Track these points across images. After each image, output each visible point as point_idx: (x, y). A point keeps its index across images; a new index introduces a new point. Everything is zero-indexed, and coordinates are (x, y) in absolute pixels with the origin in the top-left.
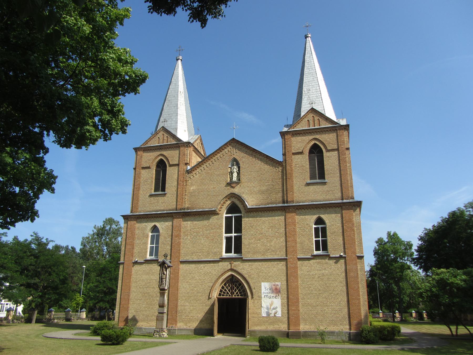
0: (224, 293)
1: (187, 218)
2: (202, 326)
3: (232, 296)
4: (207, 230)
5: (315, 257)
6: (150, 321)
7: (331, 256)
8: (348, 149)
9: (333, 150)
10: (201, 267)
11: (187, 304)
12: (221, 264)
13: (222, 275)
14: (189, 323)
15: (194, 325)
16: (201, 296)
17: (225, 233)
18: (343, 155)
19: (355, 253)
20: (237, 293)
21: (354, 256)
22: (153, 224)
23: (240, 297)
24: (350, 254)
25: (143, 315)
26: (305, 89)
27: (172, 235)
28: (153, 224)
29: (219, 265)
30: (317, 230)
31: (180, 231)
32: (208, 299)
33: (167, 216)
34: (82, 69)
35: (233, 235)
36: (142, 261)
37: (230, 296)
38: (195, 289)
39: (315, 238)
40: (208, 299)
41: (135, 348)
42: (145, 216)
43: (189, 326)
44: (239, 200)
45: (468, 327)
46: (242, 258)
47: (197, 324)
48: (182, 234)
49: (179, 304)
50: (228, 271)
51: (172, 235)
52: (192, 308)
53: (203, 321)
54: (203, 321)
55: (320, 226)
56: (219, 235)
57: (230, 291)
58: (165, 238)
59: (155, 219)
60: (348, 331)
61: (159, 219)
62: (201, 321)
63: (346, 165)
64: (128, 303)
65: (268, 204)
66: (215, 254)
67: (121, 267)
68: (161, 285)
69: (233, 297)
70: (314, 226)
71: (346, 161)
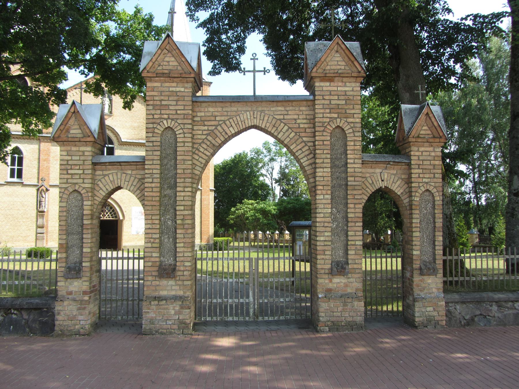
5: (8, 183)
7: (24, 183)
19: (209, 187)
20: (109, 215)
21: (208, 189)
23: (111, 218)
24: (205, 188)
25: (7, 236)
27: (39, 159)
31: (49, 156)
34: (426, 23)
36: (4, 183)
42: (16, 136)
44: (113, 132)
46: (22, 183)
48: (51, 159)
51: (39, 159)
59: (17, 140)
60: (199, 243)
61: (22, 140)
65: (139, 139)
67: (199, 193)
68: (40, 208)
69: (105, 218)
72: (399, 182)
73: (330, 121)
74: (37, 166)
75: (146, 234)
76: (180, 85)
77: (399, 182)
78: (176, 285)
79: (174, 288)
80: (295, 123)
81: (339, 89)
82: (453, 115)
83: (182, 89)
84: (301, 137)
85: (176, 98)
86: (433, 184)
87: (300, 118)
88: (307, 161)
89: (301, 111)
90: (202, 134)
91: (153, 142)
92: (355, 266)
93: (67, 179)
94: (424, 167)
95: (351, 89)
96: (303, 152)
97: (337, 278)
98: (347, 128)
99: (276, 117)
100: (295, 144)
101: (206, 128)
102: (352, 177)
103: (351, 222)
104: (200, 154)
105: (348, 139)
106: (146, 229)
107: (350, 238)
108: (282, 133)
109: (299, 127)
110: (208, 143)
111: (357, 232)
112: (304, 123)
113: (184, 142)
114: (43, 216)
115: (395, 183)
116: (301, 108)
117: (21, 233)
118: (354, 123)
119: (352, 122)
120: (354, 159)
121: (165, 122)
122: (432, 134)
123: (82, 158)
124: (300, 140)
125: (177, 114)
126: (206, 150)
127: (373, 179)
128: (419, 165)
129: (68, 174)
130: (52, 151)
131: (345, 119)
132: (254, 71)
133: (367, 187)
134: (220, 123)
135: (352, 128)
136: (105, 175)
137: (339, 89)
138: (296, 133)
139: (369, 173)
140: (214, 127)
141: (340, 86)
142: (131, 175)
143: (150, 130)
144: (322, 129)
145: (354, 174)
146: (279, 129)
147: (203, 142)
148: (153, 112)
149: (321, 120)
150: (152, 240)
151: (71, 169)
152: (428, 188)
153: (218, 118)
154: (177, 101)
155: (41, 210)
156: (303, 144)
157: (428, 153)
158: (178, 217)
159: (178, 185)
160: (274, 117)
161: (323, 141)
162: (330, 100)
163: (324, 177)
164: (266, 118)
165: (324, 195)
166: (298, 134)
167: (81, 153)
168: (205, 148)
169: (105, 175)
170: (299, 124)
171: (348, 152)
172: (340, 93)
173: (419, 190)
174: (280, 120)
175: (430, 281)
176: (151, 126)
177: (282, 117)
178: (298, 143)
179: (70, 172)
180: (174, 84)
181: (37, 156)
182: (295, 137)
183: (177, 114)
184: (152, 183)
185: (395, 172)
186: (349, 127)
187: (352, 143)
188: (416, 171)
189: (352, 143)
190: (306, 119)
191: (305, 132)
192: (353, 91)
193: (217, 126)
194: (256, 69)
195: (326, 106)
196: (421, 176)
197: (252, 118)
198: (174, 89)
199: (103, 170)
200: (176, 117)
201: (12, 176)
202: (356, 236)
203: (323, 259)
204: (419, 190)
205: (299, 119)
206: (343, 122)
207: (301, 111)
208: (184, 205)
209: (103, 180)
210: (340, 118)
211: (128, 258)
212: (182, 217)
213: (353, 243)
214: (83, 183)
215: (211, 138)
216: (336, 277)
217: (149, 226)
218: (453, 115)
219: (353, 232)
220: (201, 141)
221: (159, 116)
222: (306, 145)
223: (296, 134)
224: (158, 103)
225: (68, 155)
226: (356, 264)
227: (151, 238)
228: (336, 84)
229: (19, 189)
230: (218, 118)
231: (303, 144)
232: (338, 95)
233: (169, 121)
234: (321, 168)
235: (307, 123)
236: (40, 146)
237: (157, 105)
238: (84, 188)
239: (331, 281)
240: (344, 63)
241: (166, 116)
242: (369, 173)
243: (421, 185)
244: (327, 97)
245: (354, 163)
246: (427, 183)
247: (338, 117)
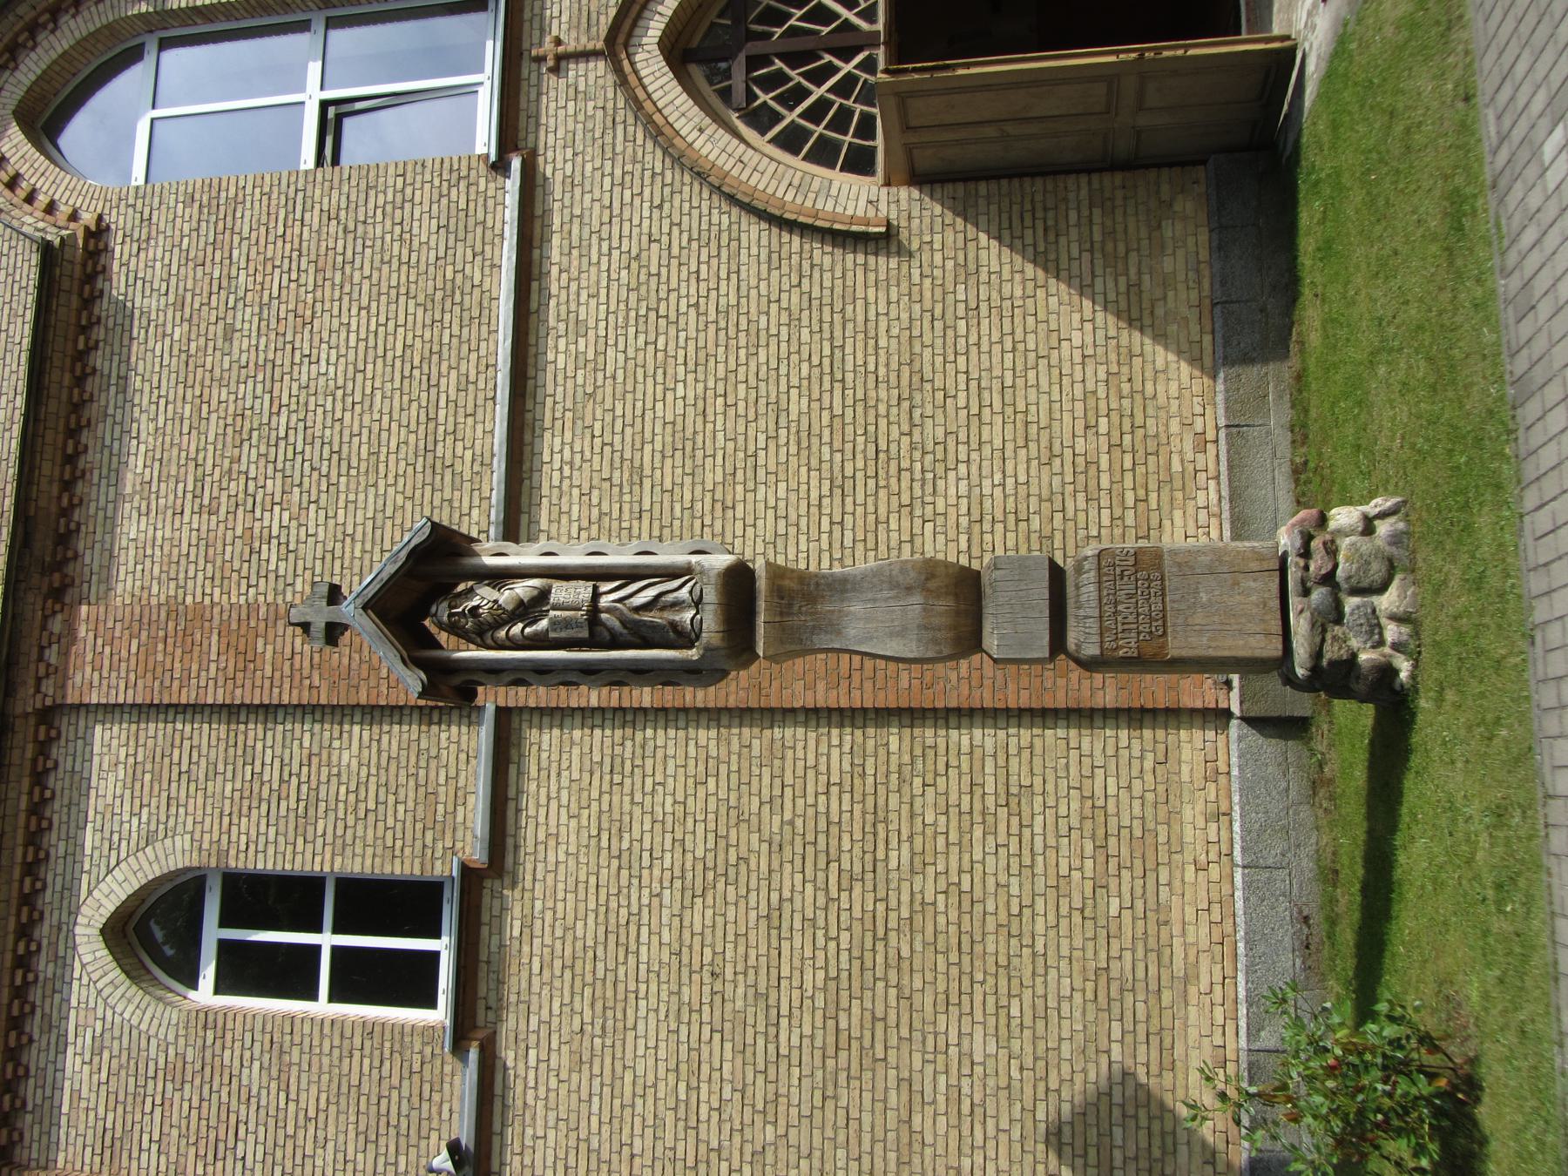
0: (840, 123)
1: (91, 559)
2: (1185, 299)
3: (871, 40)
5: (473, 1027)
6: (1160, 952)
7: (475, 850)
10: (579, 360)
11: (953, 487)
12: (555, 165)
13: (659, 133)
14: (1158, 446)
15: (1181, 393)
17: (435, 955)
22: (90, 952)
27: (231, 712)
28: (90, 952)
29: (570, 183)
30: (247, 971)
31: (200, 615)
32: (903, 252)
33: (39, 778)
36: (465, 1079)
37: (869, 65)
39: (312, 995)
40: (903, 252)
41: (1522, 962)
43: (1201, 444)
47: (1162, 356)
50: (624, 80)
51: (231, 712)
52: (994, 433)
53: (1135, 288)
54: (1135, 288)
55: (212, 933)
57: (831, 70)
58: (248, 798)
59: (44, 931)
61: (53, 876)
62: (1136, 312)
66: (461, 227)
68: (683, 638)
70: (205, 993)
74: (307, 735)
82: (550, 70)
114: (804, 595)
117: (1060, 886)
130: (160, 593)
155: (711, 623)
181: (208, 735)
201: (407, 981)
218: (550, 70)
229: (542, 918)
236: (111, 711)
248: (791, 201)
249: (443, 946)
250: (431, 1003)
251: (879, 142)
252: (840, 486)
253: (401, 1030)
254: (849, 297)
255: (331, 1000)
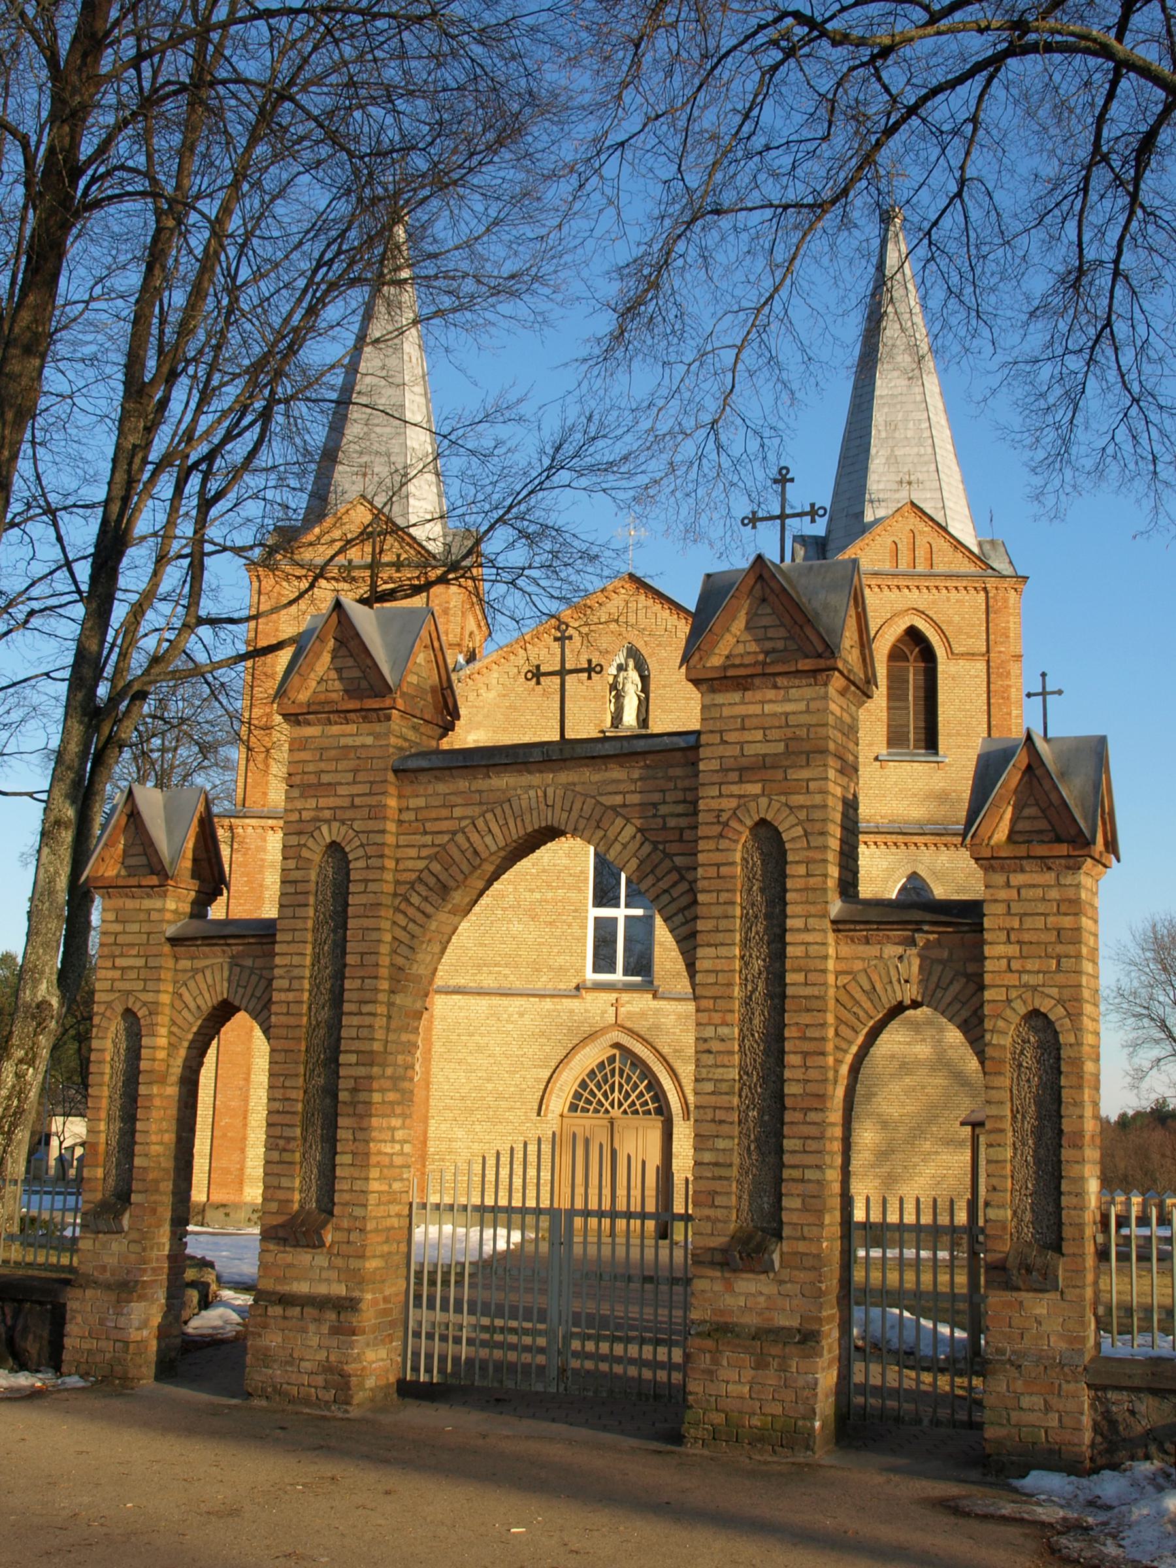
4: (532, 891)
8: (1018, 657)
9: (970, 656)
16: (510, 1109)
17: (613, 971)
18: (1000, 675)
26: (879, 417)
35: (620, 913)
38: (490, 1086)
45: (872, 633)
49: (431, 1133)
56: (576, 911)
63: (1010, 714)
64: (245, 1125)
71: (1008, 698)
72: (956, 987)
73: (739, 807)
75: (269, 1125)
76: (366, 727)
77: (956, 987)
78: (331, 1267)
79: (325, 1275)
80: (655, 816)
81: (768, 708)
83: (369, 740)
84: (669, 856)
85: (352, 764)
86: (1054, 991)
87: (668, 799)
88: (683, 924)
89: (670, 779)
90: (419, 858)
91: (295, 882)
92: (801, 1247)
93: (113, 980)
94: (1026, 937)
95: (802, 706)
96: (674, 900)
97: (748, 1280)
98: (786, 825)
99: (602, 799)
100: (651, 877)
101: (428, 839)
102: (800, 970)
103: (794, 1109)
104: (411, 911)
105: (790, 858)
106: (270, 1113)
107: (787, 1159)
108: (618, 847)
109: (664, 828)
110: (432, 881)
111: (809, 1142)
112: (679, 815)
113: (366, 881)
115: (946, 989)
116: (672, 772)
118: (806, 807)
119: (802, 807)
120: (807, 917)
121: (325, 829)
122: (1054, 830)
123: (146, 928)
124: (667, 864)
125: (353, 806)
126: (426, 899)
127: (875, 978)
128: (1009, 931)
129: (114, 967)
131: (783, 799)
132: (562, 673)
133: (857, 1002)
134: (464, 823)
135: (800, 823)
136: (195, 971)
137: (768, 708)
138: (655, 844)
139: (863, 959)
140: (446, 838)
141: (771, 701)
142: (252, 970)
143: (291, 852)
144: (717, 829)
145: (802, 962)
146: (611, 834)
147: (420, 879)
148: (299, 804)
149: (714, 804)
150: (281, 1143)
151: (122, 955)
152: (1037, 1005)
153: (458, 812)
154: (356, 771)
156: (674, 876)
157: (1040, 892)
158: (342, 1084)
159: (347, 995)
160: (598, 802)
161: (718, 865)
162: (741, 744)
163: (717, 972)
164: (577, 806)
165: (716, 1026)
166: (661, 847)
167: (143, 916)
168: (424, 894)
169: (195, 971)
170: (664, 817)
171: (790, 896)
172: (768, 722)
173: (1008, 1013)
174: (613, 808)
175: (1041, 1310)
176: (294, 840)
177: (618, 800)
178: (659, 872)
179: (119, 962)
180: (351, 728)
182: (653, 856)
183: (353, 806)
184: (289, 990)
185: (945, 955)
186: (792, 820)
187: (802, 870)
188: (1001, 950)
189: (802, 870)
190: (684, 801)
191: (681, 840)
192: (808, 711)
193: (454, 833)
194: (568, 666)
195: (730, 763)
196: (1015, 965)
197: (542, 806)
198: (349, 741)
199: (192, 958)
200: (349, 814)
201: (603, 961)
202: (805, 1152)
203: (708, 1218)
204: (1008, 1013)
205: (664, 802)
206: (775, 805)
207: (670, 779)
208: (357, 1052)
209: (191, 984)
210: (769, 796)
211: (629, 1215)
212: (351, 1084)
213: (796, 1174)
214: (144, 990)
215: (439, 867)
216: (745, 1275)
217: (277, 1105)
219: (797, 1142)
220: (414, 876)
221: (312, 814)
222: (682, 878)
223: (655, 849)
224: (313, 779)
225: (117, 921)
226: (804, 1238)
227: (280, 1137)
228: (758, 695)
230: (458, 812)
231: (674, 876)
232: (764, 729)
233: (335, 825)
234: (709, 945)
235: (686, 815)
237: (309, 786)
238: (145, 1004)
239: (729, 1288)
240: (782, 632)
241: (327, 814)
242: (863, 959)
243: (1014, 994)
244: (731, 737)
245: (807, 930)
246: (1034, 988)
247: (763, 795)
248: (556, 1086)
249: (618, 976)
250: (595, 971)
251: (1093, 1201)
252: (463, 1099)
253: (584, 958)
254: (523, 1103)
255: (616, 919)
